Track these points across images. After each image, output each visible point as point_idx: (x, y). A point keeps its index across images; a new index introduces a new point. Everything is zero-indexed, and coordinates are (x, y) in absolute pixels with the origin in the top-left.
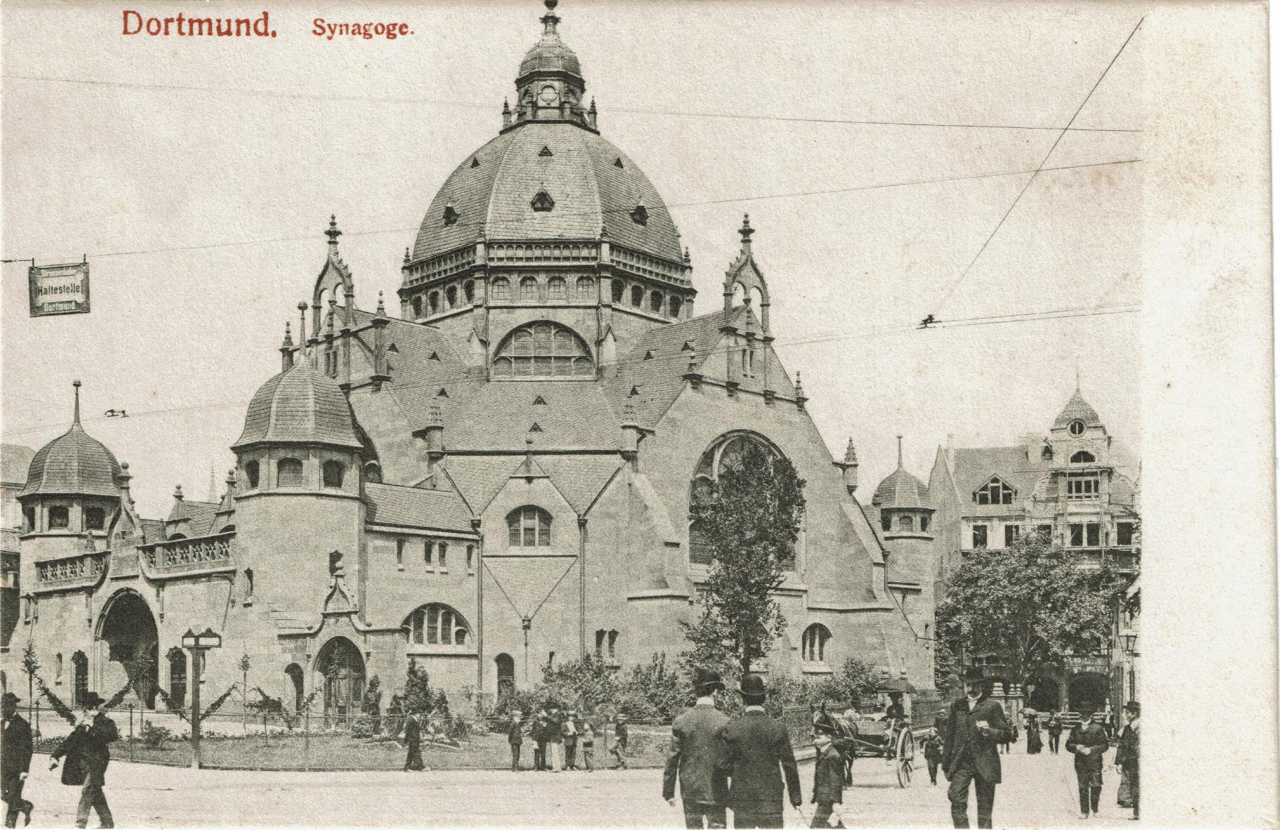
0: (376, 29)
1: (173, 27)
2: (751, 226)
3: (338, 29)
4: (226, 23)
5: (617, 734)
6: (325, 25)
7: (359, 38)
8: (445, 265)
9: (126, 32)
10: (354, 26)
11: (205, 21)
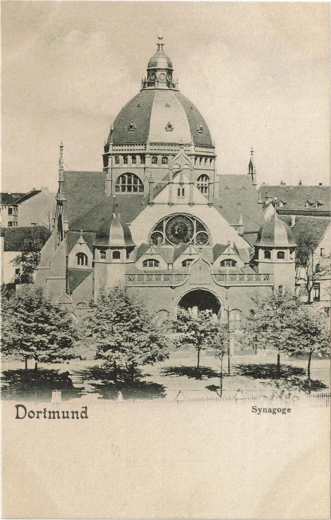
0: (278, 410)
1: (41, 416)
2: (301, 182)
3: (262, 410)
4: (60, 416)
5: (22, 314)
6: (257, 408)
7: (271, 414)
8: (206, 181)
9: (18, 417)
10: (269, 409)
11: (75, 412)
